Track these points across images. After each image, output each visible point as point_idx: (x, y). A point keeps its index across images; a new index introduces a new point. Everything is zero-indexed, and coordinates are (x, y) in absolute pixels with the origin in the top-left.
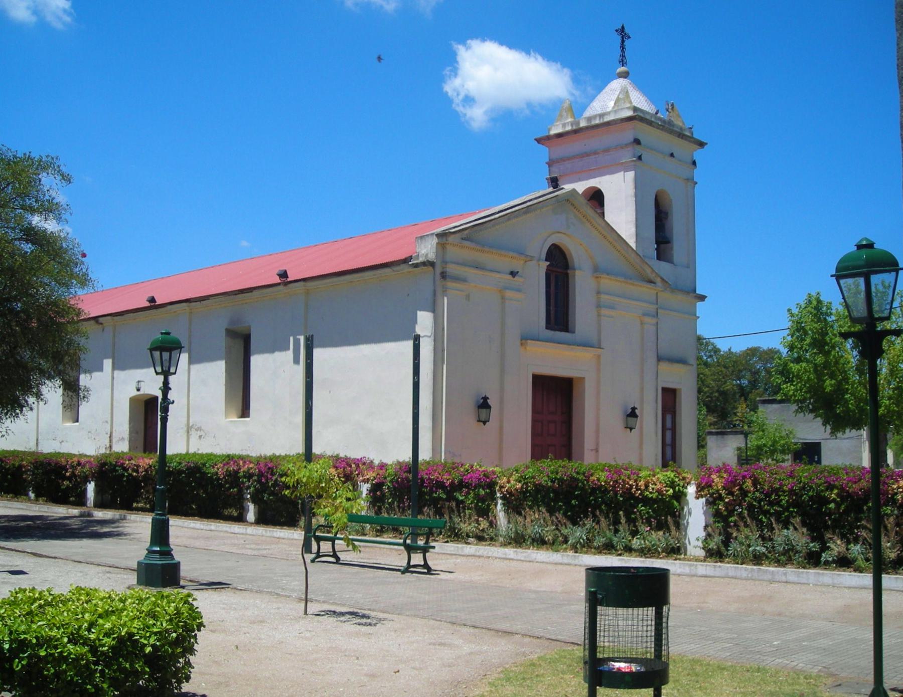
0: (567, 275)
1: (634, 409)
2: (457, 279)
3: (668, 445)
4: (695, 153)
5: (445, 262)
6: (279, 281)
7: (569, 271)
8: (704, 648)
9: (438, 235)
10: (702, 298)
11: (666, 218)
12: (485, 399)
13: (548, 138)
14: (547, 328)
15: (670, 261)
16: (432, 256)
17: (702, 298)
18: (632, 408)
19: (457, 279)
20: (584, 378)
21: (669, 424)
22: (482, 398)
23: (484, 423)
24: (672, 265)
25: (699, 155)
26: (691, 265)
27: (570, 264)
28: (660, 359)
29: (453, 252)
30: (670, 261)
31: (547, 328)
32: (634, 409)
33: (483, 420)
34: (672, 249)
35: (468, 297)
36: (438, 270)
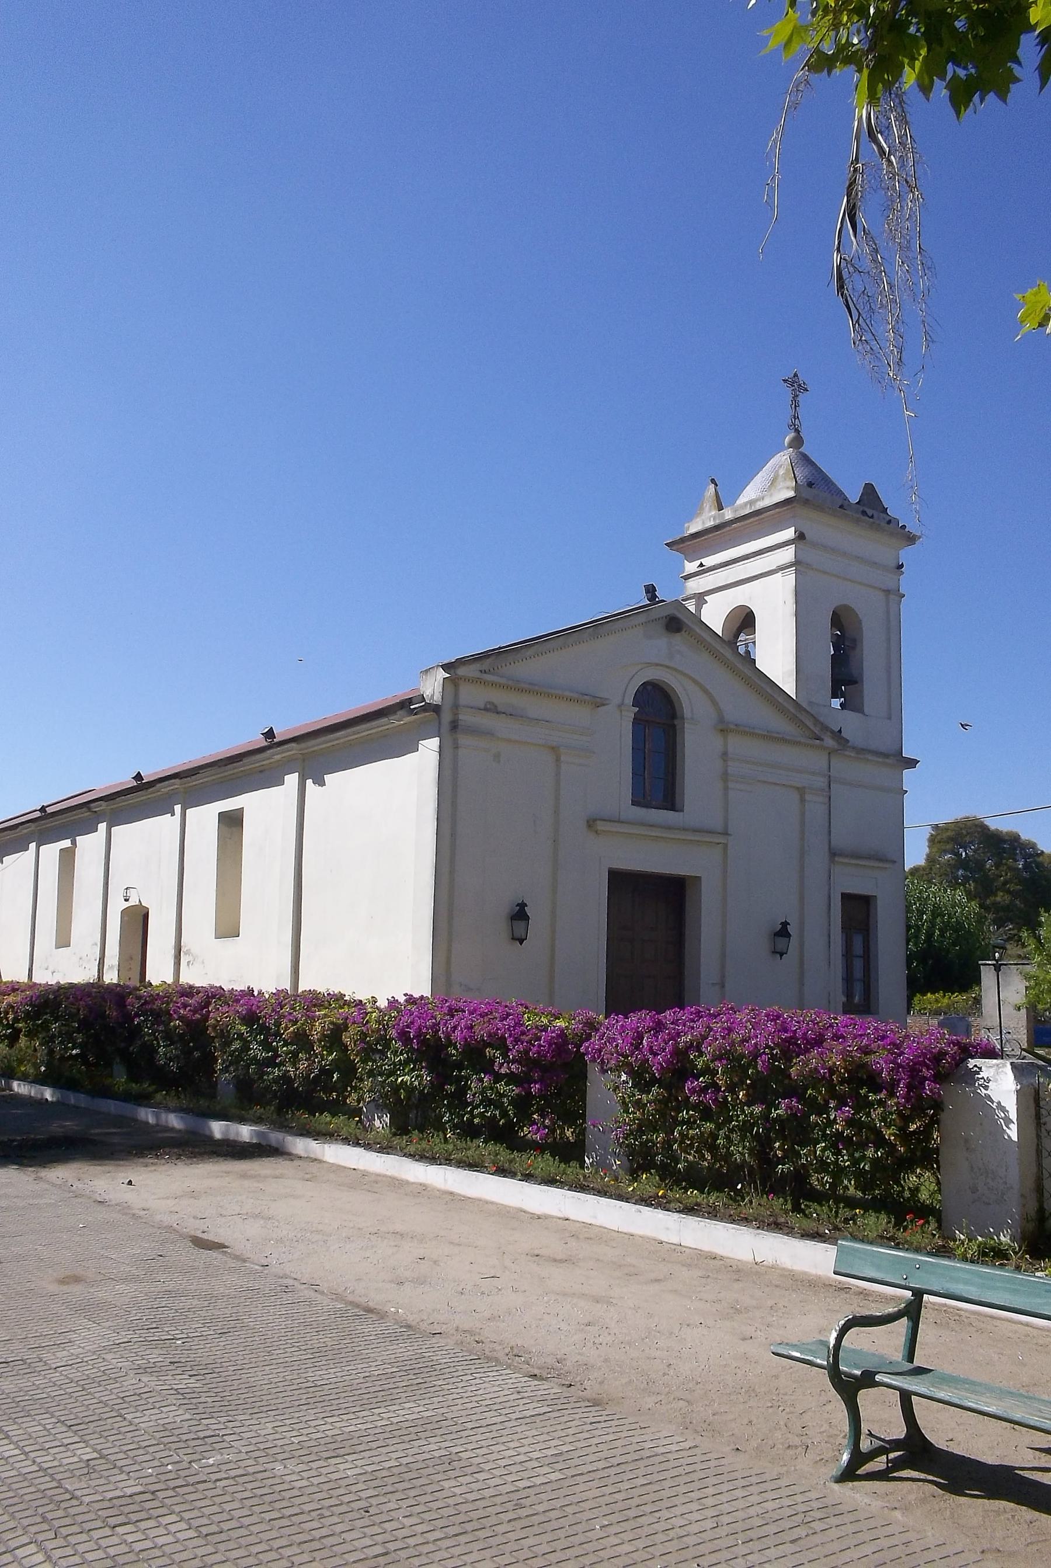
0: (674, 726)
1: (785, 924)
2: (475, 731)
3: (858, 980)
4: (900, 552)
5: (456, 707)
6: (266, 744)
7: (676, 722)
8: (300, 1305)
9: (446, 667)
10: (912, 763)
11: (854, 648)
12: (522, 906)
13: (683, 540)
14: (634, 803)
15: (859, 709)
16: (437, 699)
17: (912, 763)
18: (782, 923)
19: (475, 731)
20: (699, 878)
21: (858, 948)
22: (518, 905)
23: (521, 941)
24: (860, 715)
25: (907, 555)
26: (894, 714)
27: (678, 713)
28: (834, 854)
29: (470, 695)
30: (859, 709)
31: (634, 803)
32: (785, 924)
33: (519, 937)
34: (862, 691)
35: (497, 757)
36: (446, 717)
